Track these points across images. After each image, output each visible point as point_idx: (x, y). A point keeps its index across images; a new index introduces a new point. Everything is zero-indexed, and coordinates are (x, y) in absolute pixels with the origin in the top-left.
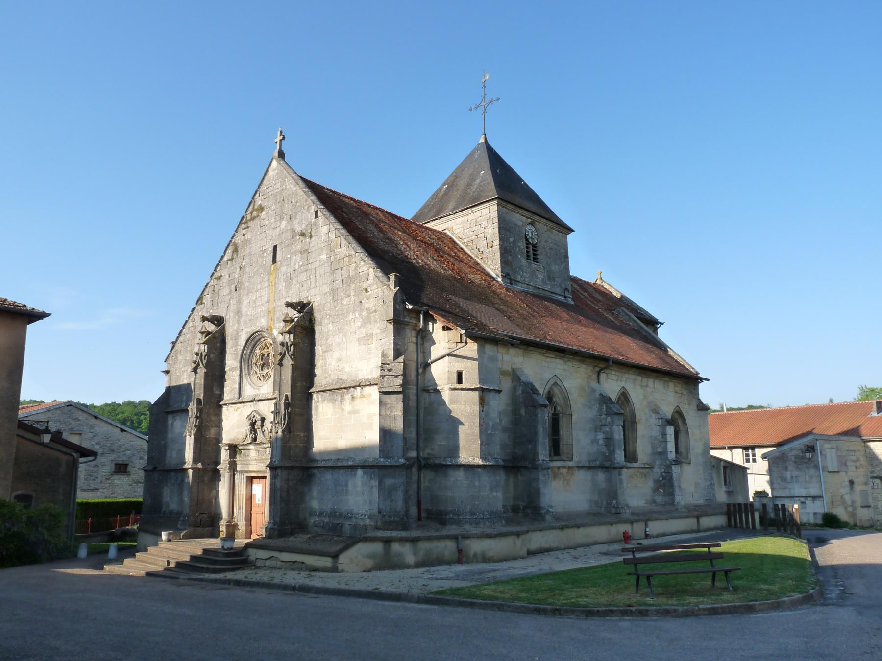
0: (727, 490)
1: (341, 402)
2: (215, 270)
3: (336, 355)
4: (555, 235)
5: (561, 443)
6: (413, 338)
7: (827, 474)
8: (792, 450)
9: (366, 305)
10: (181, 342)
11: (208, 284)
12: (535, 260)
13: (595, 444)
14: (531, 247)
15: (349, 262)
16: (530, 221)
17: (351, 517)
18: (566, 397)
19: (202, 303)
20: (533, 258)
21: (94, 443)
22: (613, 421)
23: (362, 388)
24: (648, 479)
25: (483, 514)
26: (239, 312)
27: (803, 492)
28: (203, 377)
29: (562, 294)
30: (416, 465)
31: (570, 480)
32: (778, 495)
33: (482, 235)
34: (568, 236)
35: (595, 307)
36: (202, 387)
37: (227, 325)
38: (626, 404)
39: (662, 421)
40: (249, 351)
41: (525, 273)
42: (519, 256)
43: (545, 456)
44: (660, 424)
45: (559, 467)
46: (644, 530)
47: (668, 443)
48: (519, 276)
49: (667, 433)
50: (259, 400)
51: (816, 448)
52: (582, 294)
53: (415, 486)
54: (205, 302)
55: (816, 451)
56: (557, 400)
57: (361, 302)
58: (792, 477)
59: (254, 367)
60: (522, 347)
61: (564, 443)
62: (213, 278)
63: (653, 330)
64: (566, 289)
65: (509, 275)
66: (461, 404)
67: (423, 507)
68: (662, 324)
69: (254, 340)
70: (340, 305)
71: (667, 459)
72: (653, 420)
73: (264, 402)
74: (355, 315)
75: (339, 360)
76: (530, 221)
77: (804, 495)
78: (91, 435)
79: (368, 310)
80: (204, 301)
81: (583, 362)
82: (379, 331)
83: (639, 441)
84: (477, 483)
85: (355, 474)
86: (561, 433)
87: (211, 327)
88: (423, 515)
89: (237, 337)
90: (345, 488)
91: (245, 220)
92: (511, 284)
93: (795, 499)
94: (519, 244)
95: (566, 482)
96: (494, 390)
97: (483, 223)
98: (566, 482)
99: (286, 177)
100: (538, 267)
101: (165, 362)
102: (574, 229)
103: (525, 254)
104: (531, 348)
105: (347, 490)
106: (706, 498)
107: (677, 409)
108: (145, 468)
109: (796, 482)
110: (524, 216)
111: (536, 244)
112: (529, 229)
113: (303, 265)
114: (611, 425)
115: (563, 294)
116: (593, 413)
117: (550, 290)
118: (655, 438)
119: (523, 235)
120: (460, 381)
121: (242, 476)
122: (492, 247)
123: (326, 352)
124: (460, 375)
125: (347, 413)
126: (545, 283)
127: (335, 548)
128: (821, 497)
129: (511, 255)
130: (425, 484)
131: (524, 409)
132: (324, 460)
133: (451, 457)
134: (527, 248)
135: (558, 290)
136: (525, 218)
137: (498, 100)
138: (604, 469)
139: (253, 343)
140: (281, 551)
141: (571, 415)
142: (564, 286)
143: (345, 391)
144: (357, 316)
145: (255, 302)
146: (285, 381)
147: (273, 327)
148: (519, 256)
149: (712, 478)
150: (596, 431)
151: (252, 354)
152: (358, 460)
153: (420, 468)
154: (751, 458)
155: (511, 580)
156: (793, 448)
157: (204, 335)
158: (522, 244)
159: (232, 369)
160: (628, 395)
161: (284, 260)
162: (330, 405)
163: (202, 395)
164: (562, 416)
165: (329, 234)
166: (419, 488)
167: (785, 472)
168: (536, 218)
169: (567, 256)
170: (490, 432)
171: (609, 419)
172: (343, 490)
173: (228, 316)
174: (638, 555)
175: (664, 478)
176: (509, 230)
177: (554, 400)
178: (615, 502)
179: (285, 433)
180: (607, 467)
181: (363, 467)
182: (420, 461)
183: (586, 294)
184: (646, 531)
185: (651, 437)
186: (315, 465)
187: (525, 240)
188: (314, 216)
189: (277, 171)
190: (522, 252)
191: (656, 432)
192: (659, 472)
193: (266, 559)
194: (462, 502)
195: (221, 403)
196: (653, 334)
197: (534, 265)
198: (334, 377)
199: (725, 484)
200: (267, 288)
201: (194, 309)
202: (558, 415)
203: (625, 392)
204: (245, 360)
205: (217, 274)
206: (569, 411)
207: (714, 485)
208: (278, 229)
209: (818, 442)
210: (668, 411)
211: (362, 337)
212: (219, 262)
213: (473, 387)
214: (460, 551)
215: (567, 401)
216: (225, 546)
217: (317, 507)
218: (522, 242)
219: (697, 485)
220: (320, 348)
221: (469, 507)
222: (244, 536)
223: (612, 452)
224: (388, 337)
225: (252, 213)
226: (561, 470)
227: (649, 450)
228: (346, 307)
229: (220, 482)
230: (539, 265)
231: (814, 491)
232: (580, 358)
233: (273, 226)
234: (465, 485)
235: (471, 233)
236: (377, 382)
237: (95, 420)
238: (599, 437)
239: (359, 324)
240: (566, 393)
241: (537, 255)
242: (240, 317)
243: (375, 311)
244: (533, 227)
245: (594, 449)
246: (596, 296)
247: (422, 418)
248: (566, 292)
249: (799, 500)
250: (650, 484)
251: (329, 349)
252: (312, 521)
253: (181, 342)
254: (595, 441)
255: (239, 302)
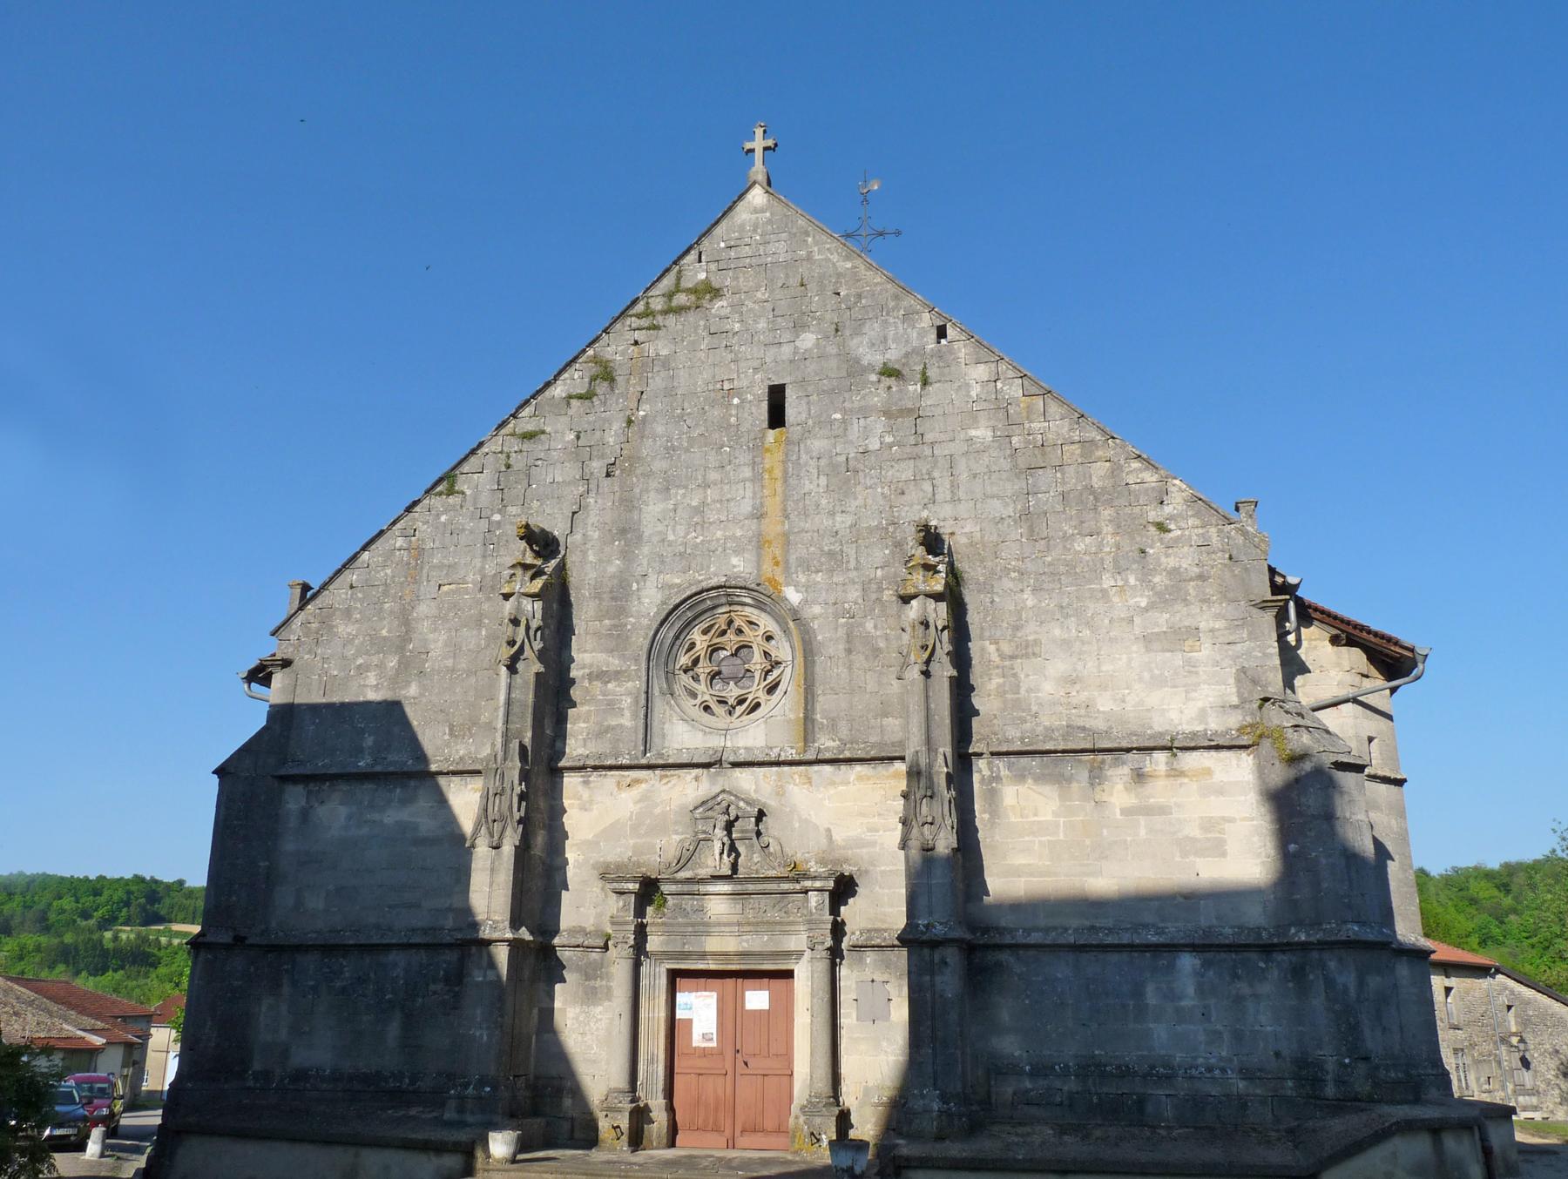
2: (514, 416)
10: (352, 587)
11: (481, 444)
17: (1169, 1077)
19: (451, 492)
23: (1175, 755)
28: (532, 686)
36: (530, 710)
40: (671, 634)
50: (736, 765)
54: (468, 492)
57: (1143, 551)
62: (503, 431)
73: (756, 769)
80: (462, 484)
89: (619, 596)
91: (640, 307)
99: (807, 234)
101: (273, 634)
121: (657, 970)
123: (1012, 657)
125: (1118, 811)
137: (898, 233)
139: (689, 614)
143: (1108, 757)
146: (936, 717)
147: (781, 579)
151: (678, 643)
152: (1174, 930)
157: (529, 573)
162: (1049, 790)
163: (529, 734)
165: (999, 385)
173: (577, 537)
174: (630, 1174)
181: (1194, 948)
186: (997, 940)
189: (768, 214)
195: (561, 764)
200: (748, 484)
201: (415, 503)
205: (526, 422)
211: (1157, 634)
212: (533, 397)
216: (855, 1168)
222: (665, 1141)
224: (1256, 639)
225: (670, 296)
229: (558, 987)
236: (480, 768)
243: (1202, 577)
252: (1010, 1090)
253: (352, 587)
255: (628, 503)
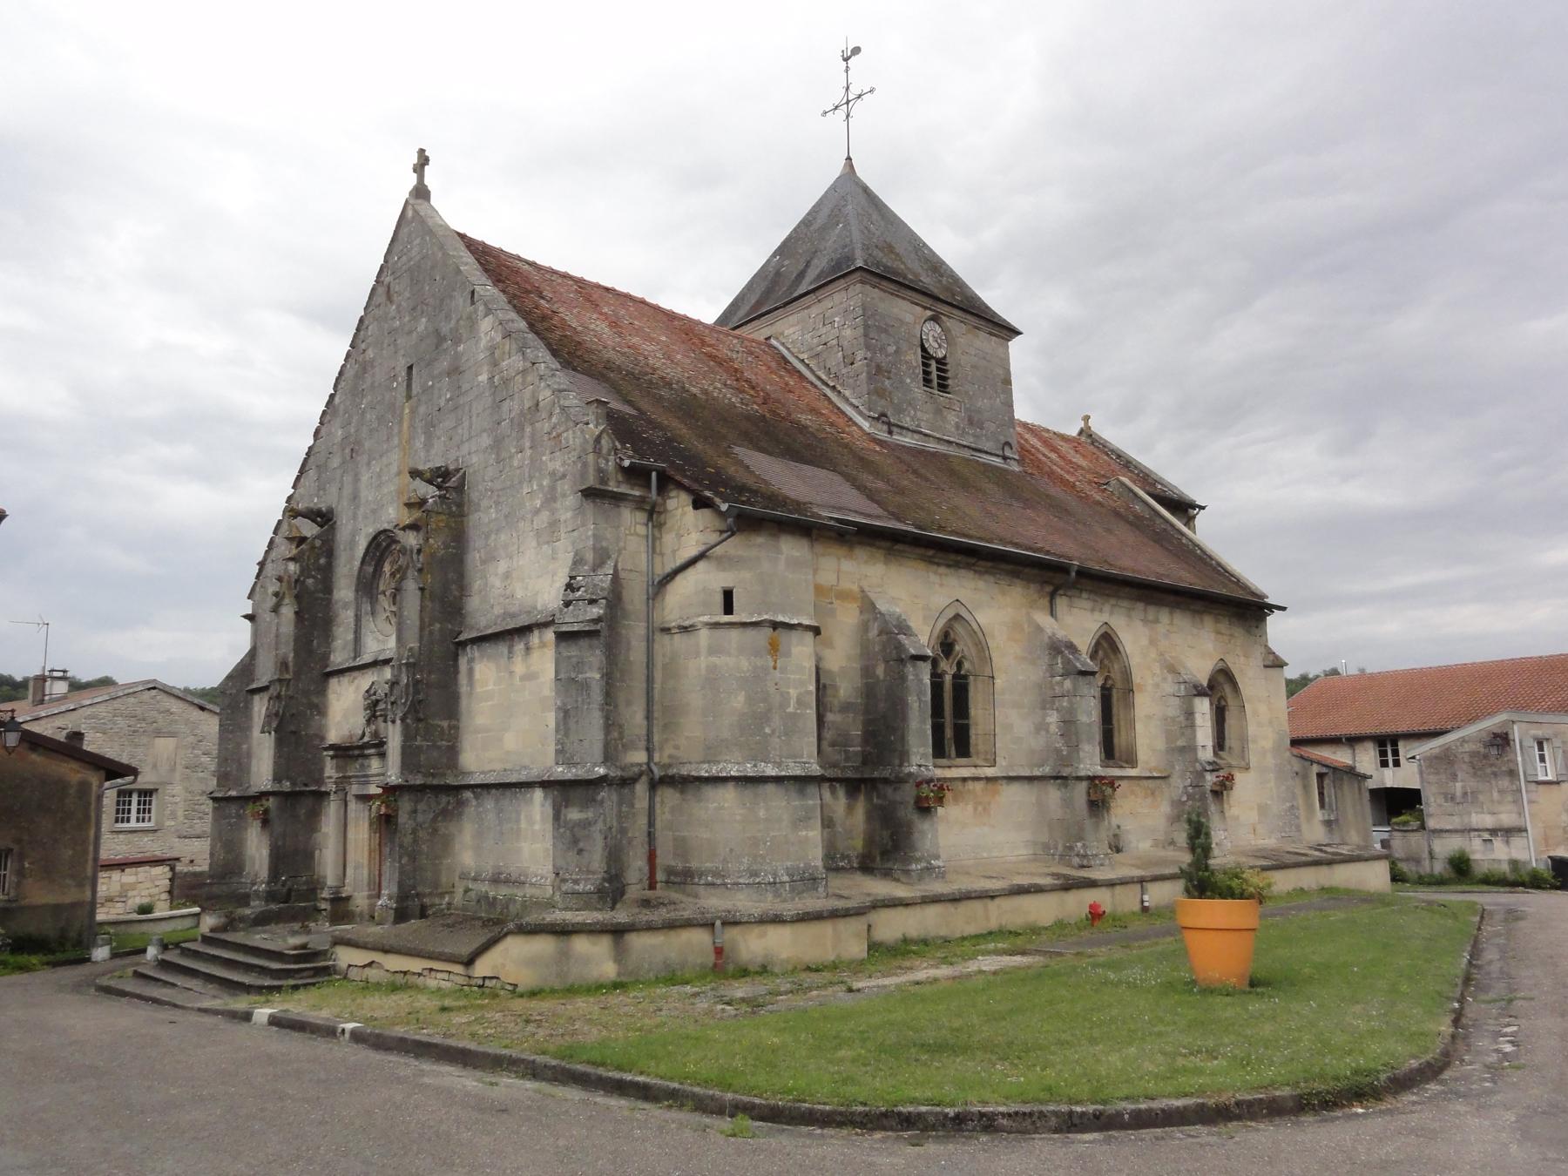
0: (1326, 818)
1: (509, 658)
3: (502, 566)
4: (983, 342)
5: (972, 732)
6: (638, 526)
7: (1533, 787)
8: (1463, 740)
9: (549, 464)
12: (943, 387)
13: (1043, 733)
14: (934, 364)
15: (524, 382)
16: (929, 313)
18: (980, 643)
20: (939, 384)
21: (200, 752)
22: (1075, 689)
24: (1159, 799)
25: (775, 875)
26: (355, 497)
27: (1488, 821)
29: (998, 453)
30: (644, 779)
31: (989, 803)
32: (1438, 827)
33: (835, 342)
34: (1010, 343)
35: (1067, 477)
37: (338, 523)
38: (1112, 657)
39: (1186, 688)
41: (919, 413)
42: (908, 381)
43: (924, 756)
44: (1183, 693)
45: (964, 780)
46: (1138, 900)
47: (1198, 729)
48: (908, 419)
49: (1196, 710)
51: (1511, 737)
52: (1044, 455)
53: (643, 821)
55: (1512, 743)
56: (965, 649)
58: (1465, 794)
59: (381, 597)
60: (1122, 605)
61: (980, 732)
63: (1185, 520)
64: (1007, 444)
65: (885, 416)
66: (729, 654)
67: (658, 861)
68: (1203, 508)
69: (381, 545)
70: (508, 469)
71: (1197, 760)
72: (1169, 687)
74: (532, 487)
75: (507, 576)
76: (929, 313)
77: (1490, 826)
78: (191, 739)
79: (553, 474)
81: (1015, 575)
82: (569, 514)
83: (1139, 727)
84: (762, 813)
85: (532, 798)
86: (972, 712)
87: (309, 529)
88: (660, 876)
89: (352, 544)
90: (515, 827)
92: (890, 432)
93: (1472, 834)
94: (908, 358)
95: (980, 808)
96: (800, 625)
97: (837, 319)
98: (980, 808)
100: (948, 401)
102: (1021, 329)
103: (921, 376)
104: (899, 547)
105: (519, 830)
106: (1283, 834)
107: (1221, 665)
108: (214, 795)
109: (1472, 802)
110: (917, 304)
111: (945, 357)
112: (932, 332)
113: (451, 399)
114: (1073, 694)
115: (1001, 453)
116: (1034, 673)
117: (973, 445)
118: (1173, 719)
119: (917, 342)
120: (728, 609)
122: (852, 364)
124: (728, 595)
126: (963, 433)
127: (465, 950)
128: (1521, 830)
129: (889, 378)
130: (663, 816)
131: (883, 666)
132: (482, 773)
133: (709, 762)
134: (924, 364)
135: (987, 446)
136: (919, 309)
138: (1059, 781)
140: (386, 951)
141: (993, 677)
142: (1002, 439)
144: (535, 487)
145: (379, 476)
148: (908, 381)
149: (1294, 797)
150: (1044, 708)
153: (654, 785)
154: (1390, 758)
155: (1424, 901)
156: (1467, 738)
158: (915, 358)
159: (346, 606)
160: (1116, 639)
161: (423, 392)
164: (975, 680)
166: (651, 823)
167: (1451, 784)
168: (945, 309)
169: (1007, 382)
170: (790, 710)
171: (1068, 684)
172: (512, 829)
175: (1190, 797)
176: (886, 331)
177: (957, 648)
178: (1079, 844)
179: (408, 721)
180: (1065, 778)
182: (651, 771)
183: (1053, 456)
184: (1142, 902)
185: (1166, 720)
187: (919, 350)
188: (469, 301)
190: (914, 373)
191: (1174, 709)
192: (1181, 786)
193: (364, 966)
194: (731, 850)
196: (1185, 529)
197: (942, 398)
198: (498, 610)
199: (1322, 806)
202: (965, 677)
203: (1110, 632)
204: (367, 587)
206: (988, 672)
207: (1298, 809)
208: (415, 334)
209: (1515, 727)
210: (1200, 669)
213: (754, 620)
214: (719, 951)
215: (984, 651)
217: (472, 864)
218: (915, 354)
219: (1263, 810)
220: (478, 555)
221: (745, 860)
223: (1074, 748)
226: (970, 785)
227: (1161, 744)
228: (518, 471)
230: (950, 399)
231: (1507, 819)
232: (1010, 567)
233: (406, 329)
234: (738, 818)
235: (815, 341)
237: (201, 712)
238: (1049, 719)
239: (538, 503)
240: (980, 634)
241: (948, 378)
242: (357, 507)
243: (564, 476)
244: (937, 326)
245: (1038, 743)
246: (1074, 460)
247: (657, 686)
248: (1006, 448)
249: (1479, 836)
250: (1165, 808)
251: (491, 558)
254: (1041, 727)
255: (356, 479)
